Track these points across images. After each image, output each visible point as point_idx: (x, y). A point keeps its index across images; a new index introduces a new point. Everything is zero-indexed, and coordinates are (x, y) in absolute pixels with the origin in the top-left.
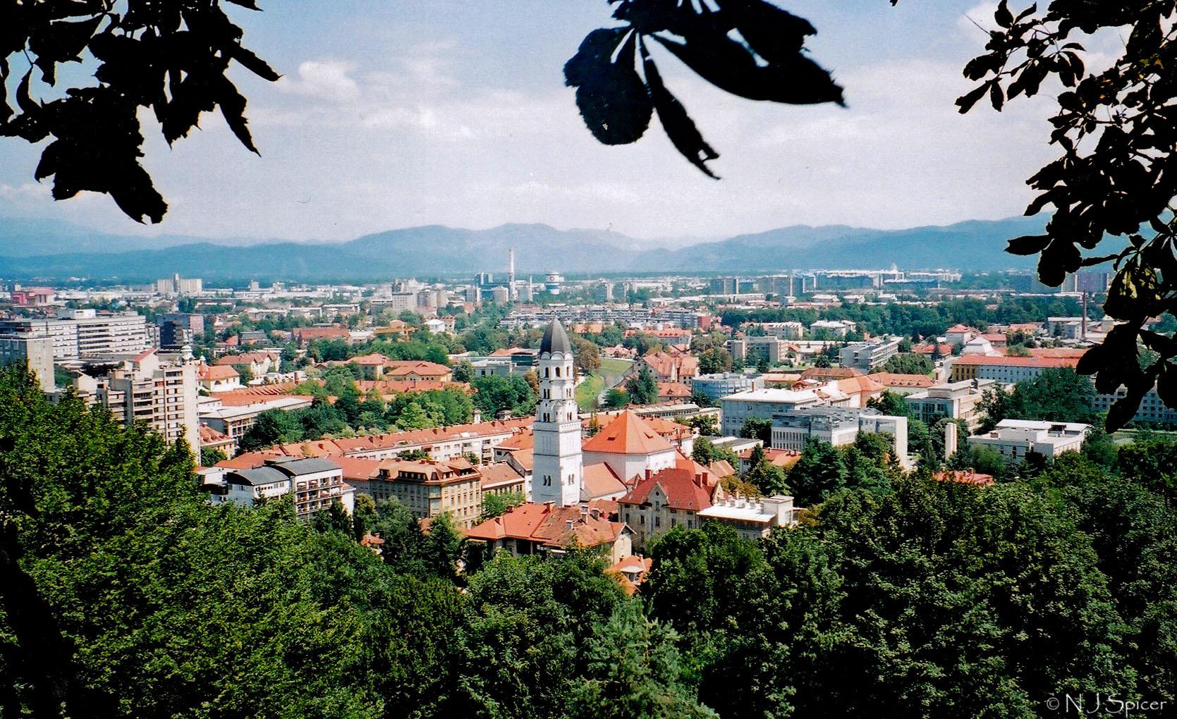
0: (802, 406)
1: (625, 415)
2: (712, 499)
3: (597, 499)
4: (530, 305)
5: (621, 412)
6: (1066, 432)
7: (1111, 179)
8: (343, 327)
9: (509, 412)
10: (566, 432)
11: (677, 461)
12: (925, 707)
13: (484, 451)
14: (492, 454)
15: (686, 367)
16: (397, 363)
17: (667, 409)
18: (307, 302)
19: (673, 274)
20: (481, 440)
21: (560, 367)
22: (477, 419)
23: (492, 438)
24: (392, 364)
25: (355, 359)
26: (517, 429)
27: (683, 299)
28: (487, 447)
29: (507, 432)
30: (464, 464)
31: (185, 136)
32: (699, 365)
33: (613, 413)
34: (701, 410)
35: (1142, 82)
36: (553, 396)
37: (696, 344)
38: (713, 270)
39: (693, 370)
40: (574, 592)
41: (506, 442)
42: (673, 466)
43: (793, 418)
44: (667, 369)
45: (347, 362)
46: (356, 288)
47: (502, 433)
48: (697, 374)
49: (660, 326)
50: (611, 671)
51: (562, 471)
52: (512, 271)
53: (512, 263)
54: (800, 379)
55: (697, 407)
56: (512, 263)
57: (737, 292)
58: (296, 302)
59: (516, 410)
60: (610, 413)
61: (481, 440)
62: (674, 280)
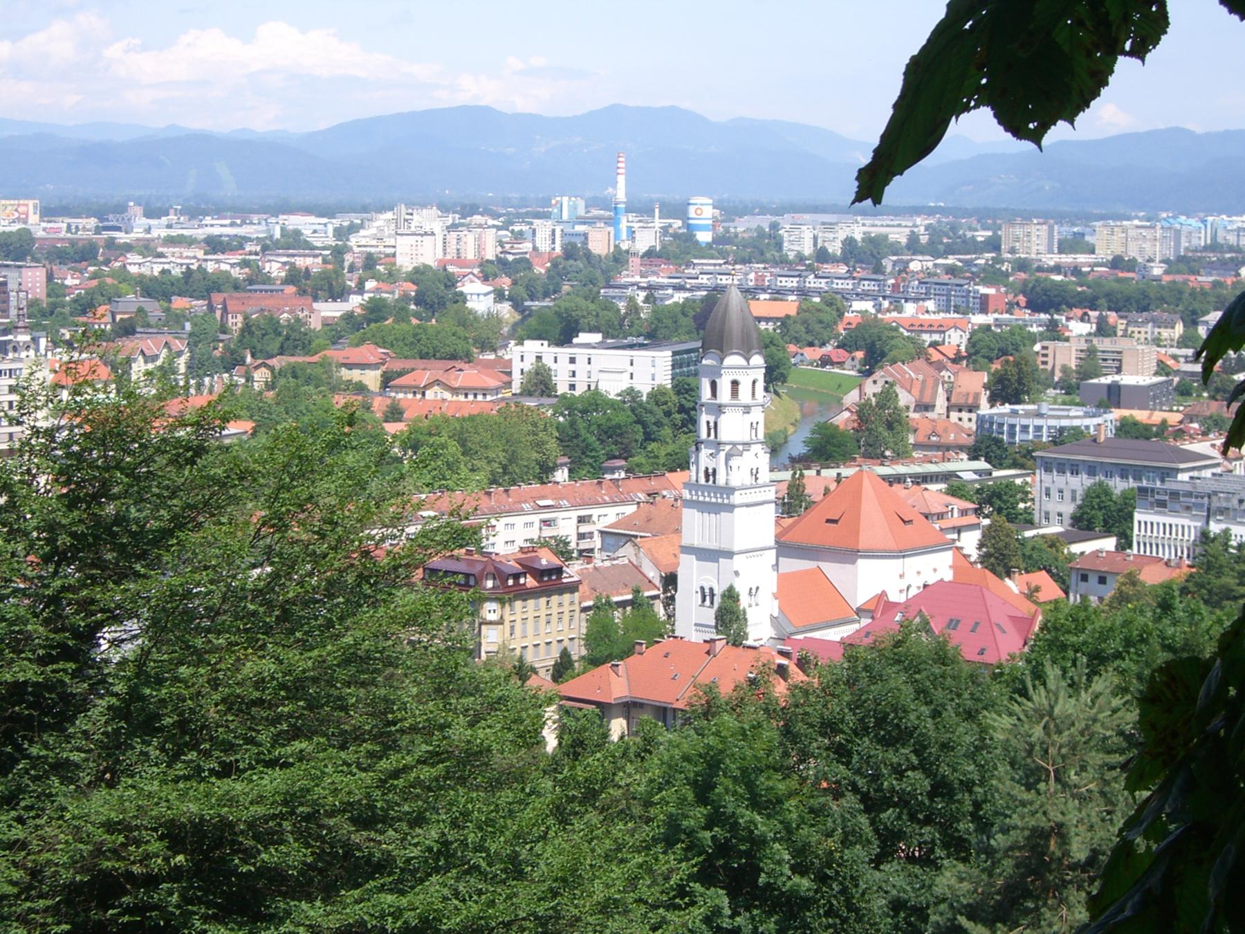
0: (1191, 474)
1: (858, 477)
5: (847, 472)
7: (971, 22)
10: (748, 505)
12: (813, 873)
13: (581, 536)
14: (597, 542)
15: (963, 390)
17: (932, 468)
18: (236, 244)
20: (574, 514)
21: (717, 380)
22: (561, 475)
23: (595, 512)
24: (397, 365)
25: (329, 353)
26: (642, 496)
27: (951, 260)
28: (584, 529)
29: (623, 502)
30: (546, 559)
34: (996, 474)
36: (724, 436)
37: (978, 346)
39: (977, 396)
40: (1095, 892)
41: (624, 521)
43: (1175, 495)
44: (928, 392)
45: (316, 358)
46: (325, 220)
47: (614, 503)
50: (452, 843)
51: (775, 590)
52: (621, 195)
53: (621, 180)
54: (1181, 422)
55: (987, 466)
57: (1056, 250)
58: (215, 245)
60: (824, 472)
61: (574, 514)
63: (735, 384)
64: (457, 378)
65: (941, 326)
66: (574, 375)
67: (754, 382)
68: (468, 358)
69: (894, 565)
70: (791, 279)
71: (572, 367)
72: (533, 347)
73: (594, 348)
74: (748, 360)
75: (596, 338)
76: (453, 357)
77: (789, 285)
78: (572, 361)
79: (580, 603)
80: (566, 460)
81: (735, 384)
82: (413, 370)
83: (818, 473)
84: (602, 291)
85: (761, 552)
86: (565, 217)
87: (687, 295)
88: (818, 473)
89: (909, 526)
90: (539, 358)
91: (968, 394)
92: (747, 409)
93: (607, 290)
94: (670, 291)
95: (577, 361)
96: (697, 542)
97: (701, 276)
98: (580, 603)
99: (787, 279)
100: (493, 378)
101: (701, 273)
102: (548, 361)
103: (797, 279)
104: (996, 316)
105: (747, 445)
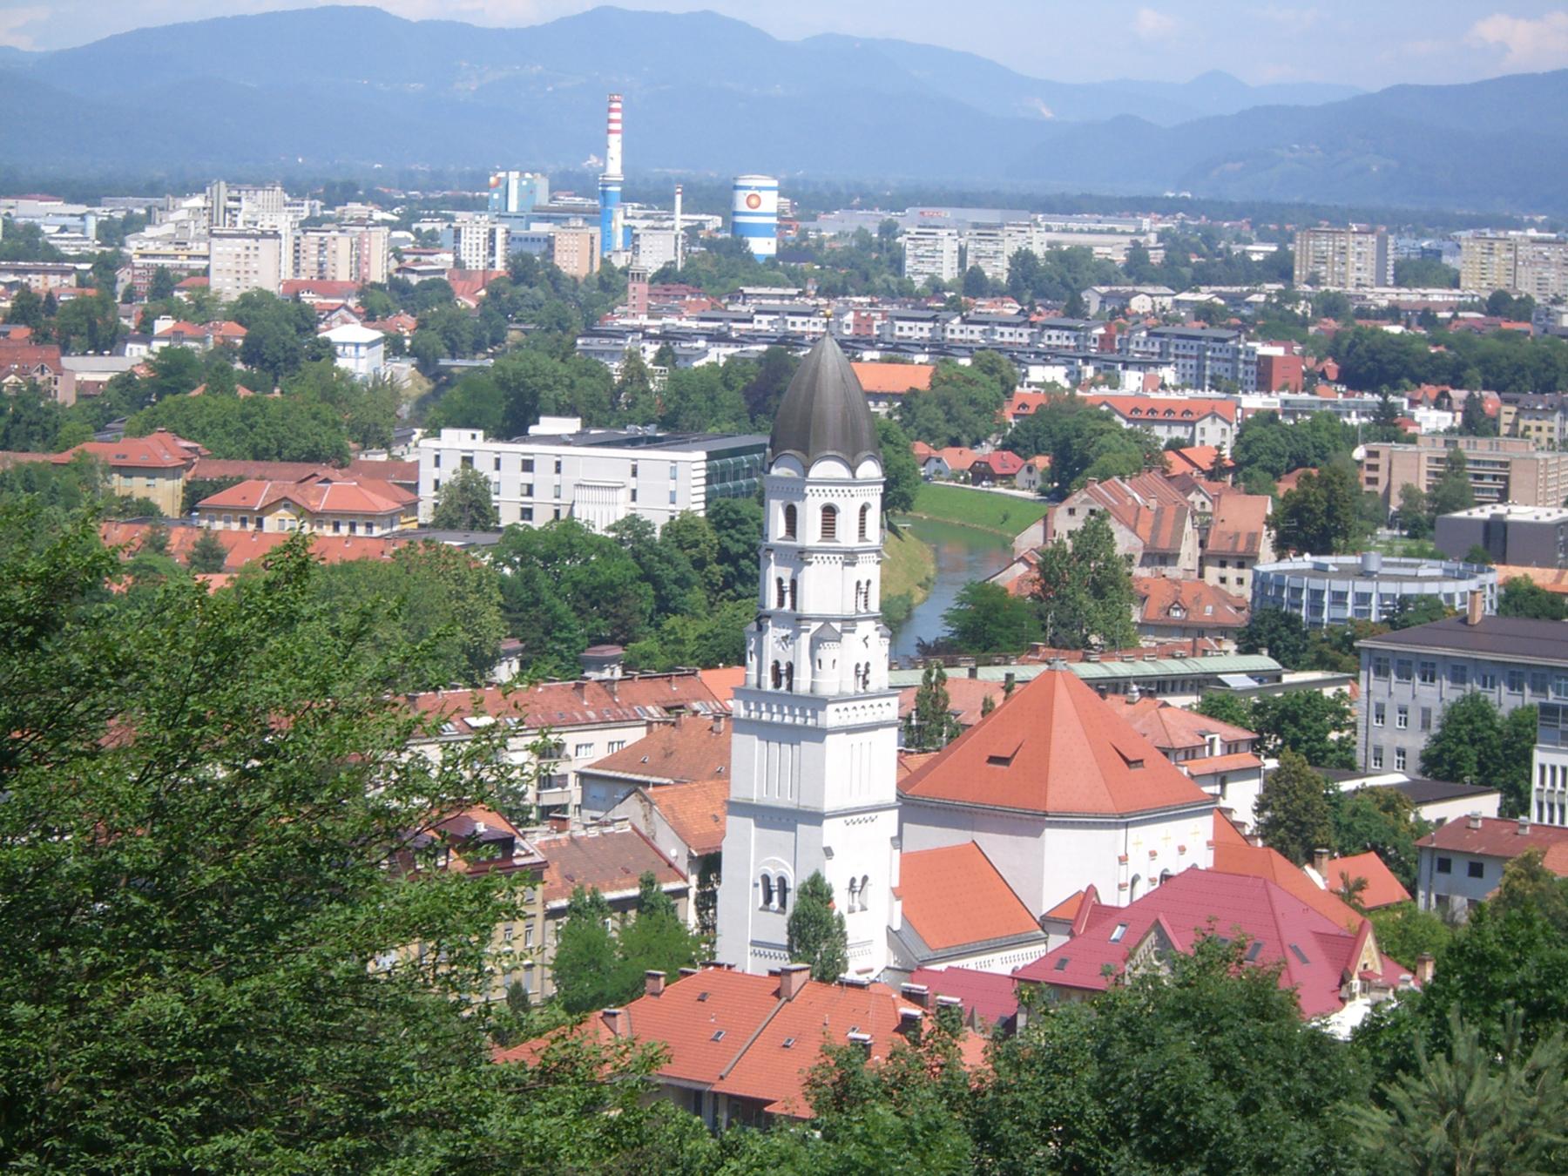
2: (1344, 981)
3: (942, 967)
4: (676, 289)
5: (1026, 671)
6: (841, 984)
8: (42, 338)
9: (616, 651)
11: (1216, 845)
15: (1228, 527)
16: (231, 469)
17: (1175, 667)
19: (1167, 208)
21: (797, 504)
24: (213, 471)
25: (88, 447)
29: (621, 722)
31: (1209, 844)
32: (1271, 522)
33: (993, 674)
34: (1287, 678)
35: (1368, 904)
38: (1297, 199)
39: (1253, 539)
42: (1205, 860)
45: (67, 457)
47: (604, 724)
48: (1266, 549)
49: (1132, 381)
55: (1272, 664)
56: (615, 144)
59: (648, 644)
60: (984, 673)
62: (1168, 224)
63: (829, 511)
64: (319, 496)
65: (1188, 412)
66: (530, 492)
67: (864, 510)
68: (339, 459)
69: (1107, 841)
70: (920, 324)
71: (527, 478)
72: (456, 440)
73: (567, 444)
74: (853, 469)
75: (571, 425)
76: (313, 457)
77: (916, 335)
78: (528, 466)
79: (545, 902)
80: (516, 644)
81: (829, 511)
82: (241, 479)
83: (973, 673)
84: (579, 341)
85: (873, 815)
86: (513, 207)
87: (732, 350)
88: (973, 673)
89: (1135, 771)
90: (467, 461)
91: (1237, 535)
92: (850, 557)
93: (588, 340)
94: (701, 344)
95: (536, 466)
96: (757, 795)
97: (757, 317)
98: (545, 902)
99: (912, 324)
100: (384, 495)
101: (758, 312)
102: (483, 466)
103: (931, 325)
104: (1285, 395)
105: (850, 622)
